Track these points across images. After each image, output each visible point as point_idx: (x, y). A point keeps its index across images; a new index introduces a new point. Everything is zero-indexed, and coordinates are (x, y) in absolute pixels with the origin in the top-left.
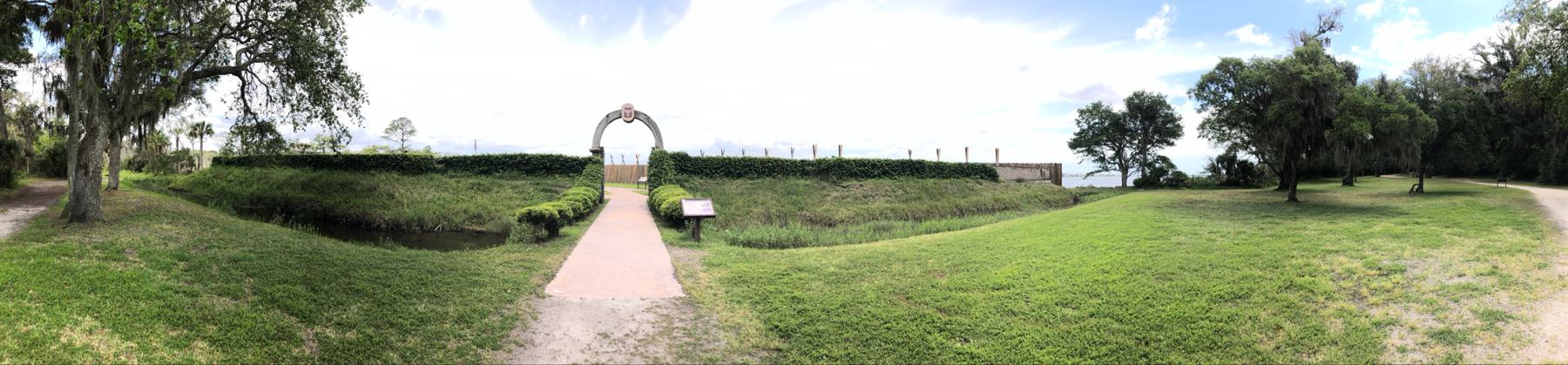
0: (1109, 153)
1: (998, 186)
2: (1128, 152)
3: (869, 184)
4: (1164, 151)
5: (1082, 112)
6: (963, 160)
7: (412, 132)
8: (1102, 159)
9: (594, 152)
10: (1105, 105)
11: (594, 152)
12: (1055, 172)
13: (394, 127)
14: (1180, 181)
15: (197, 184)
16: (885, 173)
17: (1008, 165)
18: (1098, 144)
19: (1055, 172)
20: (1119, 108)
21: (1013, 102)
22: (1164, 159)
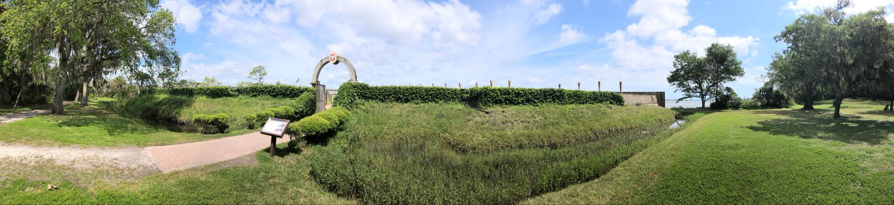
0: (692, 85)
1: (623, 108)
2: (705, 85)
3: (512, 109)
4: (726, 84)
5: (677, 57)
6: (597, 90)
7: (264, 74)
8: (688, 90)
9: (314, 85)
10: (692, 53)
11: (314, 85)
12: (661, 98)
13: (254, 72)
14: (737, 106)
15: (131, 103)
16: (528, 101)
17: (629, 93)
18: (687, 80)
19: (661, 98)
20: (702, 54)
21: (637, 63)
22: (728, 89)
